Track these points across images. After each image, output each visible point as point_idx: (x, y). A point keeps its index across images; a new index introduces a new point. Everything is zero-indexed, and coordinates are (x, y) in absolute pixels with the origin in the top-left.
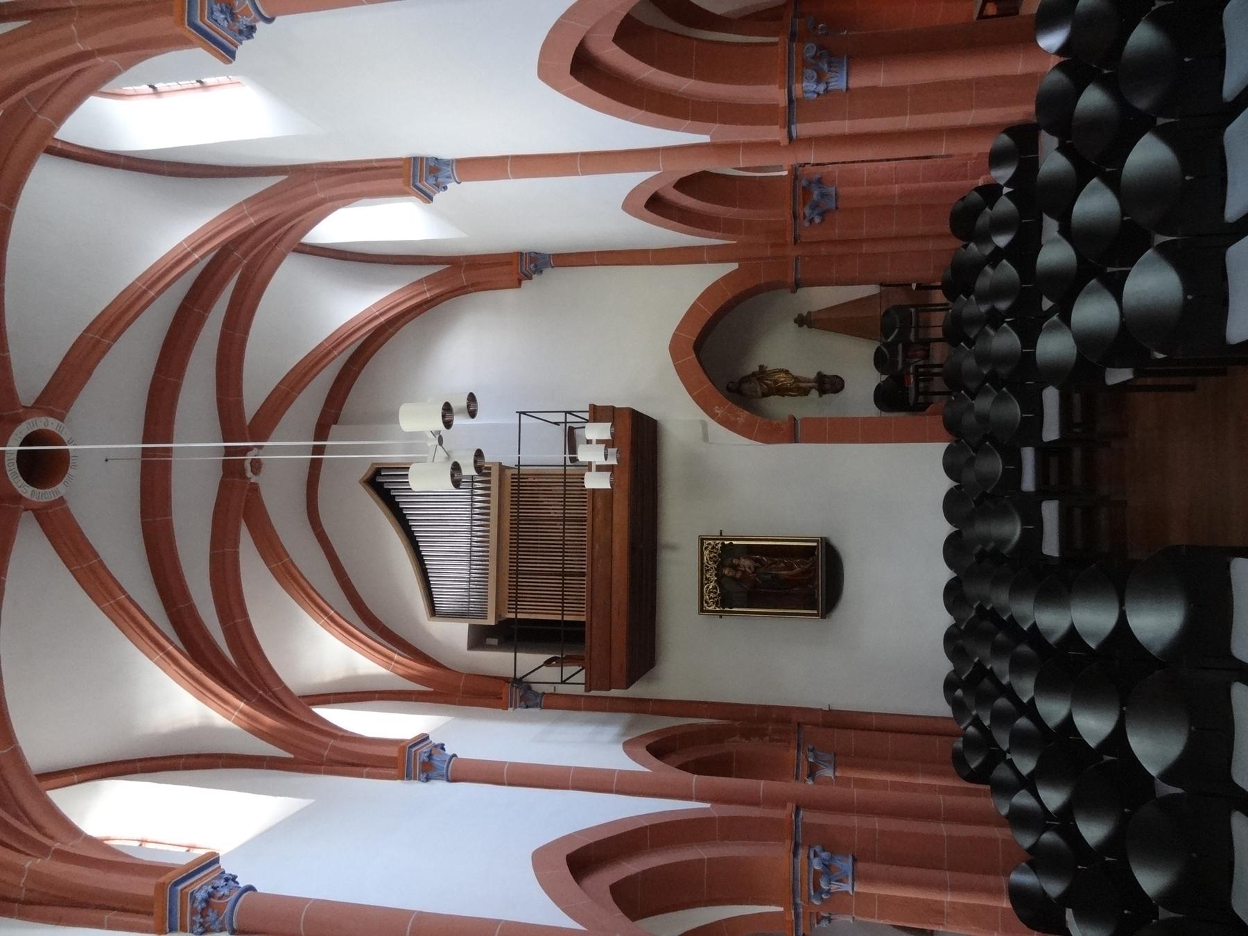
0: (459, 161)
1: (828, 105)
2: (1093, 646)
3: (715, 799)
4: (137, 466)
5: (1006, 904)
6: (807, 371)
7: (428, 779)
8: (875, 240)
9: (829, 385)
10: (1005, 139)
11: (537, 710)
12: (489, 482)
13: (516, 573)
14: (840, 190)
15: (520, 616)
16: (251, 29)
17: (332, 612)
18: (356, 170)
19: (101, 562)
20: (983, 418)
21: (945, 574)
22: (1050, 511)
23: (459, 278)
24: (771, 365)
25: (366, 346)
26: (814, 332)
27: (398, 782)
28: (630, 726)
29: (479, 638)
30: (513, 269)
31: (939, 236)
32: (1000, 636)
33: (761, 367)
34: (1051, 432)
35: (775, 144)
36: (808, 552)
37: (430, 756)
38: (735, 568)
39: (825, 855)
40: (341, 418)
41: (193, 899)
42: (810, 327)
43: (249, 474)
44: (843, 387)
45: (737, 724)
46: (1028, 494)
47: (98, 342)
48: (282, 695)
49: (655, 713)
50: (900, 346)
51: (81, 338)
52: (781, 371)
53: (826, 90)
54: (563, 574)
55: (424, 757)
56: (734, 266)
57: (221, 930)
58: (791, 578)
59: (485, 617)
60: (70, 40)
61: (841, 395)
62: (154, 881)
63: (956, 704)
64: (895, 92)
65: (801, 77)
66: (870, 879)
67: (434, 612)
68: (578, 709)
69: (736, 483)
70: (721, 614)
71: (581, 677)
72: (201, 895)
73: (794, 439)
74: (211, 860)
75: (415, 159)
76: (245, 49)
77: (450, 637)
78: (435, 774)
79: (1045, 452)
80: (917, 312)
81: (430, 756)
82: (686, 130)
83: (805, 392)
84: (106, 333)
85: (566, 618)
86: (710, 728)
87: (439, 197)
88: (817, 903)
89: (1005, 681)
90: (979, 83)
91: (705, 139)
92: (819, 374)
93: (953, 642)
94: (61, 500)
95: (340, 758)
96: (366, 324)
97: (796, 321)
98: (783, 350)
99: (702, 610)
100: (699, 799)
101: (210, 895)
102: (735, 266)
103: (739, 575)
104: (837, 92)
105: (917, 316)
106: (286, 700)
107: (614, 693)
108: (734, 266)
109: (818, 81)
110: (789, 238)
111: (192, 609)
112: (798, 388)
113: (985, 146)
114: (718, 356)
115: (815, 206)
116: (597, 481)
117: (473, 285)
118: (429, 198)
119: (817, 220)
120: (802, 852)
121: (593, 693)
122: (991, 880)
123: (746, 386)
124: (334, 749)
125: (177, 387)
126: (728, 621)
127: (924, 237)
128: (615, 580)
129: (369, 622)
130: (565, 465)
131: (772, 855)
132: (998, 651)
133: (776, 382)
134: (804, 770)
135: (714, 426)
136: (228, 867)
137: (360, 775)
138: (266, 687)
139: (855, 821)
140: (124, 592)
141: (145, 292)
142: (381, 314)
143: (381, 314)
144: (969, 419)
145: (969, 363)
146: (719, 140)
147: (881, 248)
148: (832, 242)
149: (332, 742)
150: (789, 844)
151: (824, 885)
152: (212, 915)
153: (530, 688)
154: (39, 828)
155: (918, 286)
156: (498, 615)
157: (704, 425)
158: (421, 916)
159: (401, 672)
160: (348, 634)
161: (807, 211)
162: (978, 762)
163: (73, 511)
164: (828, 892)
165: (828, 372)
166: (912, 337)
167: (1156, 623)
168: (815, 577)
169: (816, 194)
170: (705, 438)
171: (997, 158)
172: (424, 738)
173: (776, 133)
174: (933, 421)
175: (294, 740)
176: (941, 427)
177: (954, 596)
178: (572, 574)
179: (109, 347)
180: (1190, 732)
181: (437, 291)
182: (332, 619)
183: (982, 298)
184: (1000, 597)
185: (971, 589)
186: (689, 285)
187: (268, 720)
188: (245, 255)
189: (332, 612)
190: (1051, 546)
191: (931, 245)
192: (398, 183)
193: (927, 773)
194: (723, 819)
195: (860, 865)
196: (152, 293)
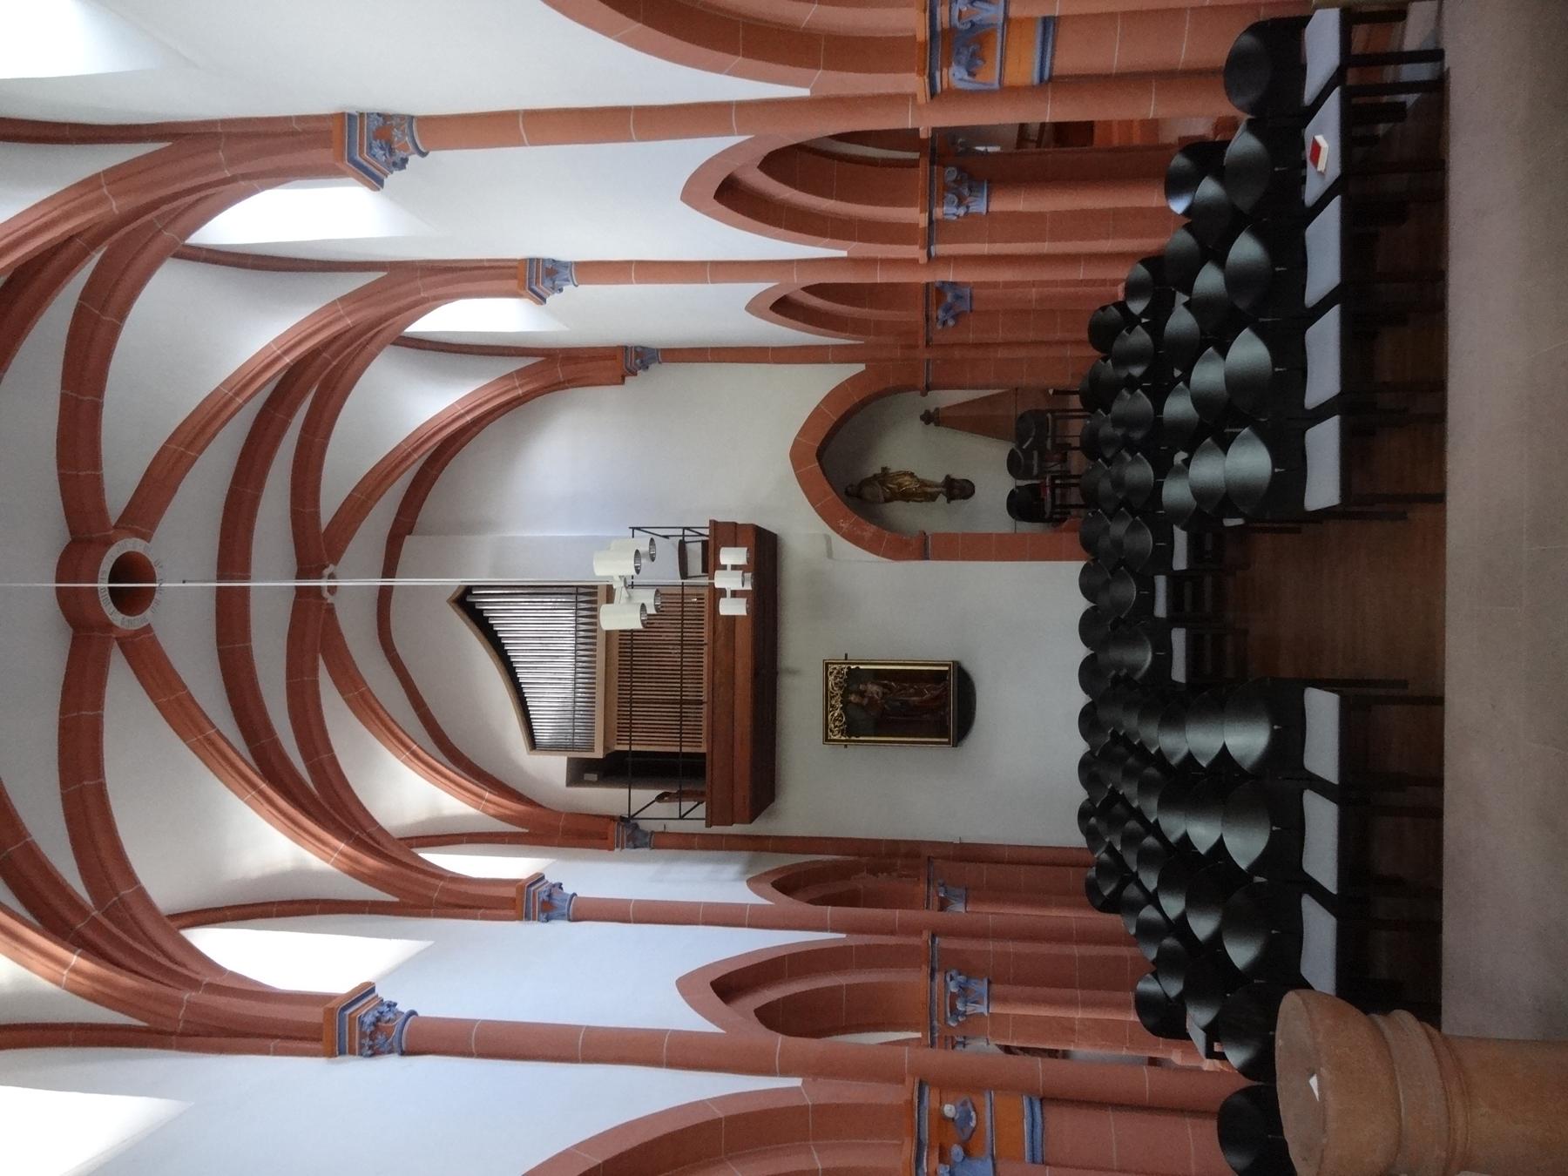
0: (577, 264)
1: (970, 227)
2: (1204, 764)
3: (850, 929)
4: (292, 598)
5: (1133, 1017)
6: (934, 474)
7: (548, 919)
8: (1008, 344)
9: (958, 490)
10: (1142, 272)
11: (646, 850)
14: (975, 291)
15: (634, 748)
16: (405, 161)
17: (415, 747)
18: (463, 269)
19: (189, 695)
20: (1118, 544)
21: (1081, 699)
22: (1179, 637)
23: (558, 371)
24: (894, 468)
25: (444, 449)
26: (943, 430)
27: (516, 923)
28: (750, 865)
29: (580, 772)
30: (617, 364)
31: (1078, 343)
32: (1131, 760)
33: (884, 469)
34: (1180, 562)
35: (914, 262)
36: (938, 677)
37: (550, 896)
38: (862, 694)
39: (961, 978)
41: (362, 1023)
42: (937, 424)
44: (973, 486)
45: (864, 860)
46: (1158, 619)
47: (182, 455)
48: (378, 837)
49: (776, 851)
50: (1036, 454)
51: (163, 449)
52: (906, 474)
53: (966, 214)
54: (682, 702)
55: (544, 896)
56: (860, 368)
57: (390, 1052)
58: (921, 705)
59: (592, 749)
60: (217, 167)
61: (972, 500)
62: (321, 1010)
63: (1089, 832)
64: (1038, 217)
65: (942, 201)
66: (1004, 1000)
67: (533, 744)
69: (869, 604)
70: (846, 744)
71: (701, 811)
72: (369, 1019)
73: (924, 556)
74: (367, 991)
75: (531, 260)
76: (394, 179)
77: (553, 768)
78: (555, 913)
79: (1176, 580)
80: (1055, 419)
81: (550, 896)
82: (826, 246)
83: (932, 498)
84: (189, 445)
85: (685, 750)
86: (835, 866)
87: (553, 299)
88: (953, 1025)
89: (1135, 805)
90: (1116, 213)
91: (844, 254)
92: (948, 477)
93: (1089, 770)
94: (148, 629)
95: (452, 900)
96: (453, 421)
97: (922, 418)
98: (910, 450)
99: (827, 740)
100: (834, 930)
101: (378, 1019)
102: (861, 367)
103: (865, 701)
104: (977, 215)
105: (1055, 426)
106: (383, 840)
107: (736, 829)
108: (861, 367)
109: (958, 206)
110: (922, 342)
111: (276, 743)
112: (923, 493)
113: (1122, 273)
114: (845, 471)
115: (948, 309)
116: (732, 608)
117: (569, 381)
118: (541, 299)
119: (951, 323)
120: (938, 977)
121: (716, 830)
122: (1119, 995)
123: (867, 491)
124: (445, 891)
125: (255, 501)
126: (852, 749)
127: (1062, 343)
129: (454, 758)
131: (913, 979)
132: (1129, 774)
133: (900, 485)
134: (935, 902)
135: (837, 540)
136: (384, 993)
137: (475, 918)
139: (991, 946)
140: (213, 726)
141: (231, 400)
142: (468, 412)
143: (468, 412)
144: (1104, 543)
145: (1105, 486)
146: (855, 255)
147: (1022, 353)
148: (963, 345)
150: (926, 970)
151: (960, 1007)
152: (380, 1038)
153: (636, 826)
154: (184, 966)
155: (1056, 392)
156: (605, 748)
157: (828, 540)
158: (590, 1030)
161: (941, 314)
162: (1108, 887)
163: (160, 639)
164: (964, 1014)
165: (958, 474)
166: (1049, 446)
167: (1247, 740)
168: (946, 705)
169: (949, 298)
170: (830, 554)
171: (1133, 289)
172: (539, 878)
173: (915, 252)
174: (1071, 539)
175: (401, 884)
176: (1078, 548)
177: (1089, 721)
178: (689, 702)
179: (195, 460)
180: (1272, 834)
181: (526, 389)
183: (1117, 422)
184: (1130, 722)
185: (1104, 714)
186: (811, 387)
187: (371, 862)
188: (334, 357)
189: (415, 747)
190: (1179, 673)
191: (1068, 352)
192: (512, 284)
193: (1060, 905)
194: (857, 947)
195: (995, 987)
196: (239, 400)
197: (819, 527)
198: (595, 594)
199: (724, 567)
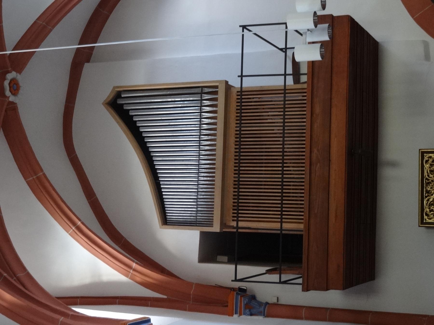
11: (261, 318)
12: (216, 99)
13: (238, 184)
17: (79, 223)
40: (92, 58)
43: (8, 93)
59: (211, 225)
67: (165, 221)
68: (300, 318)
77: (182, 244)
128: (332, 182)
130: (285, 75)
138: (14, 274)
149: (62, 319)
156: (223, 224)
157: (426, 45)
159: (138, 279)
160: (92, 243)
170: (427, 57)
182: (79, 228)
189: (79, 223)
197: (419, 34)
198: (216, 93)
199: (243, 31)
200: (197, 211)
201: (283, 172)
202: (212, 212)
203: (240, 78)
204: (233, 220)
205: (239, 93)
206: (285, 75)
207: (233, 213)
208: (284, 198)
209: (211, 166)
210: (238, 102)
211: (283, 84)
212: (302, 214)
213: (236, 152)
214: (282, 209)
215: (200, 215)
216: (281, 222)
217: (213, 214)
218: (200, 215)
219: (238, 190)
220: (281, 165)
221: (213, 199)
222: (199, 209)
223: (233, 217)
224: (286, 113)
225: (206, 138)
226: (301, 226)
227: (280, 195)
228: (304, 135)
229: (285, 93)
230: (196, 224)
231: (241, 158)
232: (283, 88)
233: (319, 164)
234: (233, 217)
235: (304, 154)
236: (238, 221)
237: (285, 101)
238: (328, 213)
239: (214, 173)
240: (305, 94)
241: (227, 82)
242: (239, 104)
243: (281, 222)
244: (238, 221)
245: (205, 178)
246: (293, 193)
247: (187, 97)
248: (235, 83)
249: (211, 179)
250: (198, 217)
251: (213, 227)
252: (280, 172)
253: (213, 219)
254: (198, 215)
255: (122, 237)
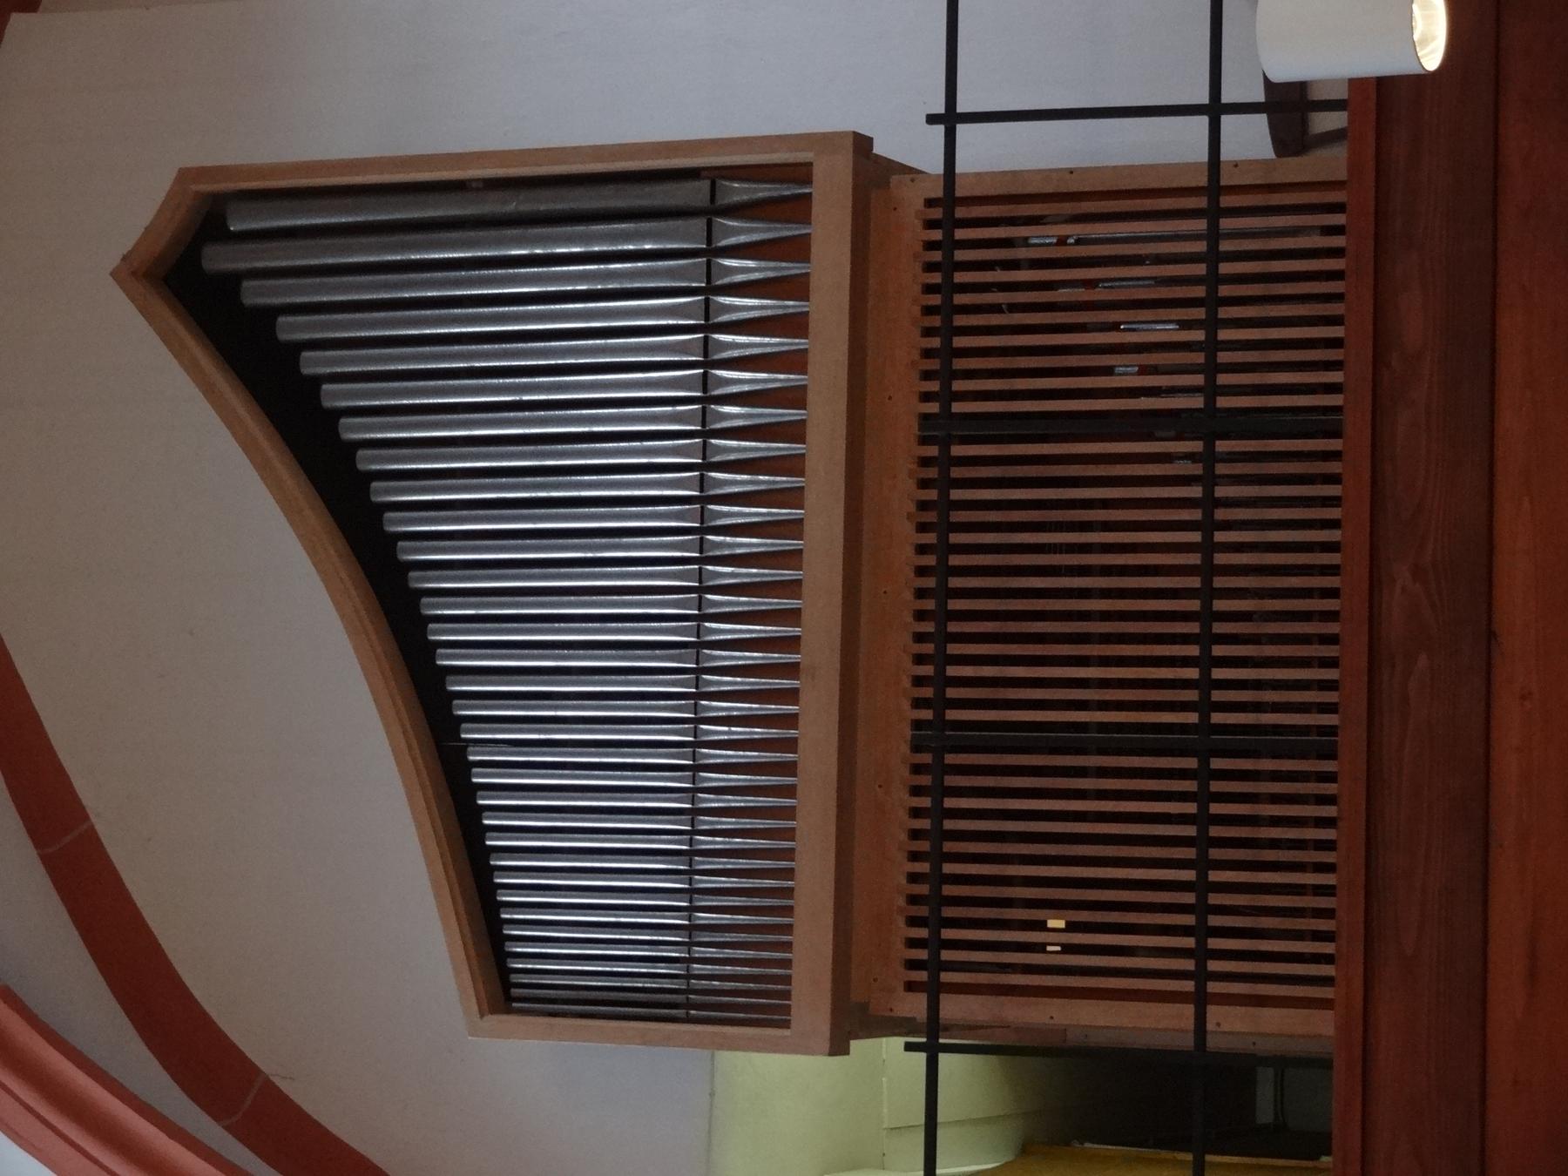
12: (795, 287)
130: (1215, 109)
198: (798, 208)
200: (691, 929)
201: (1206, 627)
202: (785, 938)
203: (940, 130)
204: (910, 987)
205: (937, 213)
206: (1215, 109)
207: (912, 943)
208: (1216, 786)
209: (775, 657)
210: (930, 267)
211: (1204, 157)
212: (1328, 948)
213: (921, 571)
214: (1202, 921)
215: (711, 952)
216: (1201, 1001)
217: (787, 946)
218: (711, 952)
219: (943, 583)
220: (1193, 650)
221: (789, 854)
222: (703, 917)
223: (913, 965)
224: (1220, 605)
225: (740, 482)
226: (1323, 1024)
227: (1190, 831)
228: (1334, 467)
229: (1214, 213)
230: (690, 1005)
231: (955, 605)
232: (1203, 181)
233: (1423, 661)
234: (913, 965)
235: (1333, 513)
236: (934, 991)
237: (1213, 257)
238: (1485, 988)
239: (791, 696)
240: (1338, 219)
241: (862, 144)
242: (925, 802)
243: (1201, 1001)
244: (934, 991)
245: (739, 732)
246: (1276, 821)
247: (627, 237)
248: (913, 146)
249: (773, 733)
250: (697, 968)
251: (785, 1024)
252: (1192, 695)
253: (787, 980)
254: (699, 952)
255: (247, 1070)
